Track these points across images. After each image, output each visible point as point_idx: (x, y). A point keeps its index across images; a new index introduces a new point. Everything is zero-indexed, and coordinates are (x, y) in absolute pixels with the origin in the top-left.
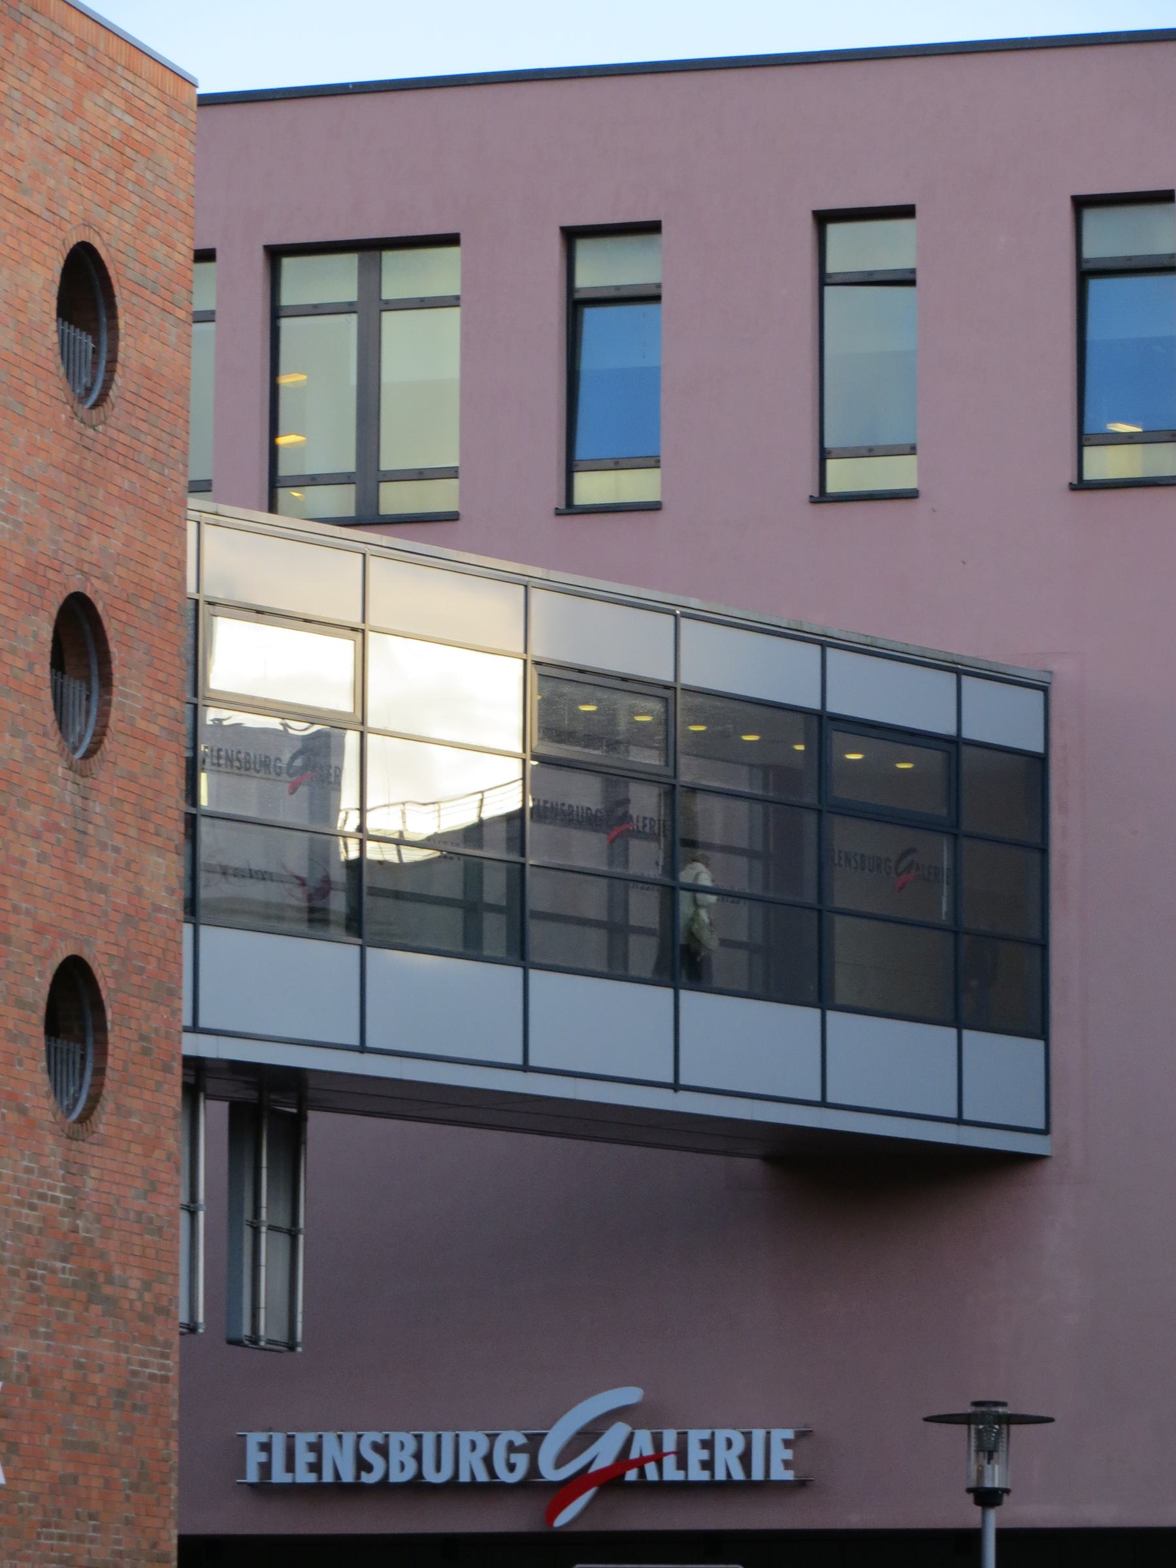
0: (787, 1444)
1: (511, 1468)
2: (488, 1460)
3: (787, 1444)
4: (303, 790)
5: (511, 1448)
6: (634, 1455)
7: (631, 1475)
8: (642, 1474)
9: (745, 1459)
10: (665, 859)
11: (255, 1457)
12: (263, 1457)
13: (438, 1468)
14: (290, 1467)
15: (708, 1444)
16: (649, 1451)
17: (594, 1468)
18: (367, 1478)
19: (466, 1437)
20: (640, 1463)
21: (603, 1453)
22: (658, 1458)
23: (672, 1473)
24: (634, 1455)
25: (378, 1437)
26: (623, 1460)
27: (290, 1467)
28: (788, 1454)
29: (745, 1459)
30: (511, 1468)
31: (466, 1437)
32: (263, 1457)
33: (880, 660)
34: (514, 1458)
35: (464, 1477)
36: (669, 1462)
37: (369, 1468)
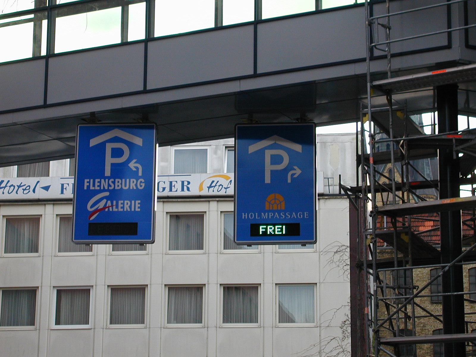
0: (139, 203)
1: (141, 186)
2: (136, 185)
3: (139, 203)
4: (350, 188)
5: (141, 182)
6: (107, 206)
7: (107, 210)
8: (109, 209)
9: (130, 207)
10: (454, 338)
11: (86, 184)
12: (88, 184)
13: (125, 186)
14: (94, 186)
15: (123, 204)
16: (110, 205)
17: (99, 208)
18: (110, 188)
19: (132, 180)
20: (109, 207)
21: (101, 205)
22: (112, 206)
23: (115, 209)
24: (107, 206)
25: (113, 180)
26: (105, 207)
27: (94, 186)
28: (139, 205)
29: (130, 207)
30: (141, 186)
31: (132, 180)
32: (88, 184)
33: (304, 66)
34: (141, 184)
35: (131, 188)
36: (114, 207)
37: (111, 186)
